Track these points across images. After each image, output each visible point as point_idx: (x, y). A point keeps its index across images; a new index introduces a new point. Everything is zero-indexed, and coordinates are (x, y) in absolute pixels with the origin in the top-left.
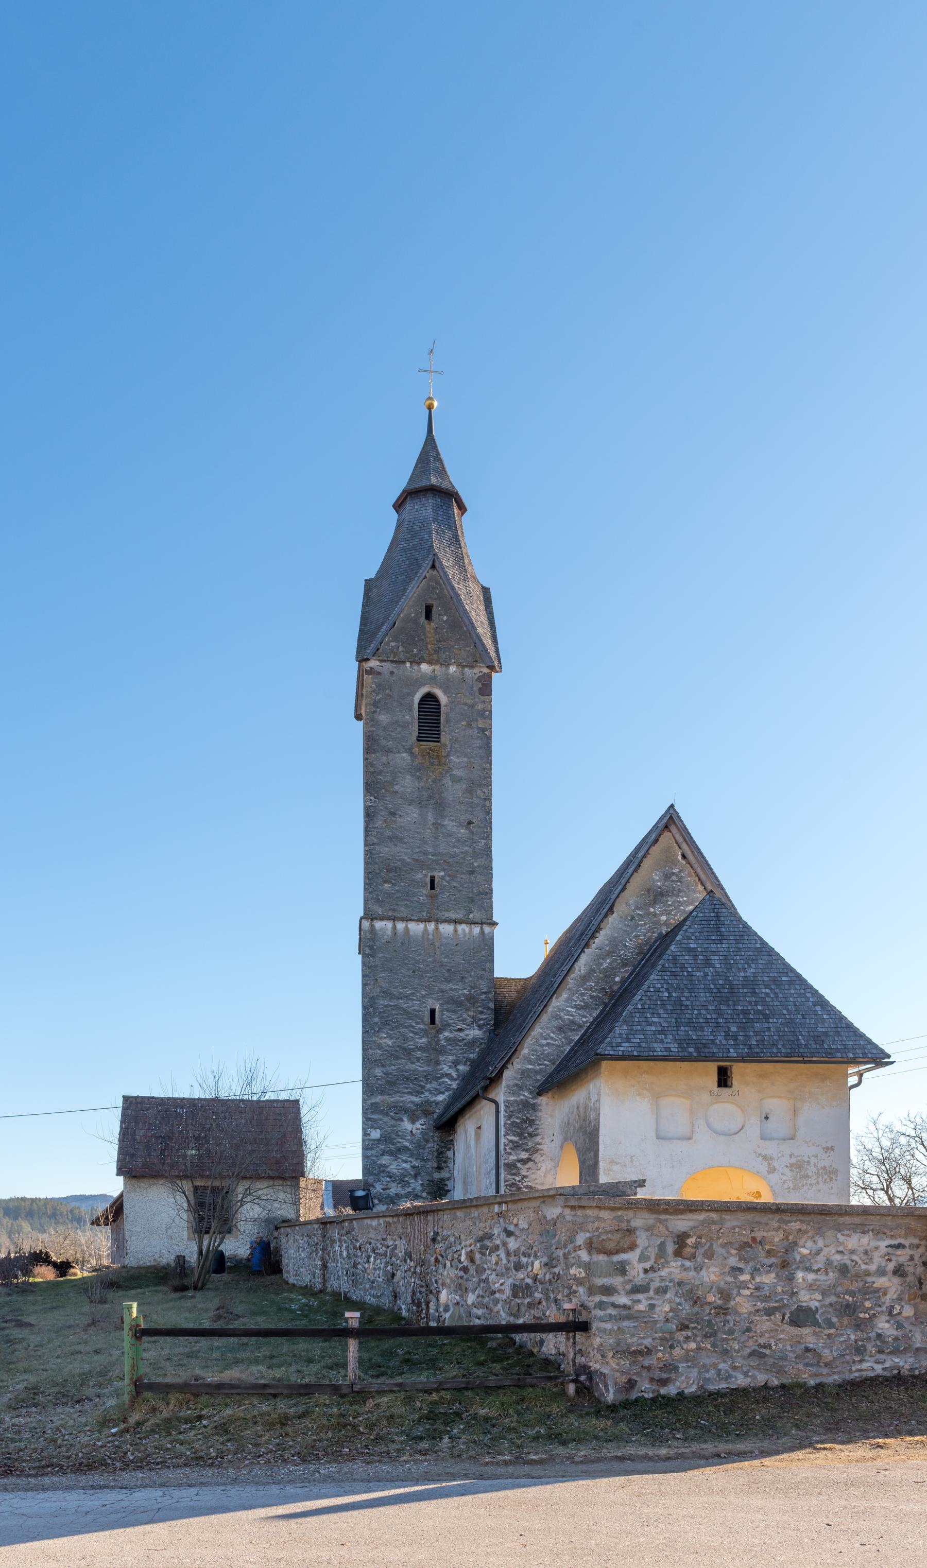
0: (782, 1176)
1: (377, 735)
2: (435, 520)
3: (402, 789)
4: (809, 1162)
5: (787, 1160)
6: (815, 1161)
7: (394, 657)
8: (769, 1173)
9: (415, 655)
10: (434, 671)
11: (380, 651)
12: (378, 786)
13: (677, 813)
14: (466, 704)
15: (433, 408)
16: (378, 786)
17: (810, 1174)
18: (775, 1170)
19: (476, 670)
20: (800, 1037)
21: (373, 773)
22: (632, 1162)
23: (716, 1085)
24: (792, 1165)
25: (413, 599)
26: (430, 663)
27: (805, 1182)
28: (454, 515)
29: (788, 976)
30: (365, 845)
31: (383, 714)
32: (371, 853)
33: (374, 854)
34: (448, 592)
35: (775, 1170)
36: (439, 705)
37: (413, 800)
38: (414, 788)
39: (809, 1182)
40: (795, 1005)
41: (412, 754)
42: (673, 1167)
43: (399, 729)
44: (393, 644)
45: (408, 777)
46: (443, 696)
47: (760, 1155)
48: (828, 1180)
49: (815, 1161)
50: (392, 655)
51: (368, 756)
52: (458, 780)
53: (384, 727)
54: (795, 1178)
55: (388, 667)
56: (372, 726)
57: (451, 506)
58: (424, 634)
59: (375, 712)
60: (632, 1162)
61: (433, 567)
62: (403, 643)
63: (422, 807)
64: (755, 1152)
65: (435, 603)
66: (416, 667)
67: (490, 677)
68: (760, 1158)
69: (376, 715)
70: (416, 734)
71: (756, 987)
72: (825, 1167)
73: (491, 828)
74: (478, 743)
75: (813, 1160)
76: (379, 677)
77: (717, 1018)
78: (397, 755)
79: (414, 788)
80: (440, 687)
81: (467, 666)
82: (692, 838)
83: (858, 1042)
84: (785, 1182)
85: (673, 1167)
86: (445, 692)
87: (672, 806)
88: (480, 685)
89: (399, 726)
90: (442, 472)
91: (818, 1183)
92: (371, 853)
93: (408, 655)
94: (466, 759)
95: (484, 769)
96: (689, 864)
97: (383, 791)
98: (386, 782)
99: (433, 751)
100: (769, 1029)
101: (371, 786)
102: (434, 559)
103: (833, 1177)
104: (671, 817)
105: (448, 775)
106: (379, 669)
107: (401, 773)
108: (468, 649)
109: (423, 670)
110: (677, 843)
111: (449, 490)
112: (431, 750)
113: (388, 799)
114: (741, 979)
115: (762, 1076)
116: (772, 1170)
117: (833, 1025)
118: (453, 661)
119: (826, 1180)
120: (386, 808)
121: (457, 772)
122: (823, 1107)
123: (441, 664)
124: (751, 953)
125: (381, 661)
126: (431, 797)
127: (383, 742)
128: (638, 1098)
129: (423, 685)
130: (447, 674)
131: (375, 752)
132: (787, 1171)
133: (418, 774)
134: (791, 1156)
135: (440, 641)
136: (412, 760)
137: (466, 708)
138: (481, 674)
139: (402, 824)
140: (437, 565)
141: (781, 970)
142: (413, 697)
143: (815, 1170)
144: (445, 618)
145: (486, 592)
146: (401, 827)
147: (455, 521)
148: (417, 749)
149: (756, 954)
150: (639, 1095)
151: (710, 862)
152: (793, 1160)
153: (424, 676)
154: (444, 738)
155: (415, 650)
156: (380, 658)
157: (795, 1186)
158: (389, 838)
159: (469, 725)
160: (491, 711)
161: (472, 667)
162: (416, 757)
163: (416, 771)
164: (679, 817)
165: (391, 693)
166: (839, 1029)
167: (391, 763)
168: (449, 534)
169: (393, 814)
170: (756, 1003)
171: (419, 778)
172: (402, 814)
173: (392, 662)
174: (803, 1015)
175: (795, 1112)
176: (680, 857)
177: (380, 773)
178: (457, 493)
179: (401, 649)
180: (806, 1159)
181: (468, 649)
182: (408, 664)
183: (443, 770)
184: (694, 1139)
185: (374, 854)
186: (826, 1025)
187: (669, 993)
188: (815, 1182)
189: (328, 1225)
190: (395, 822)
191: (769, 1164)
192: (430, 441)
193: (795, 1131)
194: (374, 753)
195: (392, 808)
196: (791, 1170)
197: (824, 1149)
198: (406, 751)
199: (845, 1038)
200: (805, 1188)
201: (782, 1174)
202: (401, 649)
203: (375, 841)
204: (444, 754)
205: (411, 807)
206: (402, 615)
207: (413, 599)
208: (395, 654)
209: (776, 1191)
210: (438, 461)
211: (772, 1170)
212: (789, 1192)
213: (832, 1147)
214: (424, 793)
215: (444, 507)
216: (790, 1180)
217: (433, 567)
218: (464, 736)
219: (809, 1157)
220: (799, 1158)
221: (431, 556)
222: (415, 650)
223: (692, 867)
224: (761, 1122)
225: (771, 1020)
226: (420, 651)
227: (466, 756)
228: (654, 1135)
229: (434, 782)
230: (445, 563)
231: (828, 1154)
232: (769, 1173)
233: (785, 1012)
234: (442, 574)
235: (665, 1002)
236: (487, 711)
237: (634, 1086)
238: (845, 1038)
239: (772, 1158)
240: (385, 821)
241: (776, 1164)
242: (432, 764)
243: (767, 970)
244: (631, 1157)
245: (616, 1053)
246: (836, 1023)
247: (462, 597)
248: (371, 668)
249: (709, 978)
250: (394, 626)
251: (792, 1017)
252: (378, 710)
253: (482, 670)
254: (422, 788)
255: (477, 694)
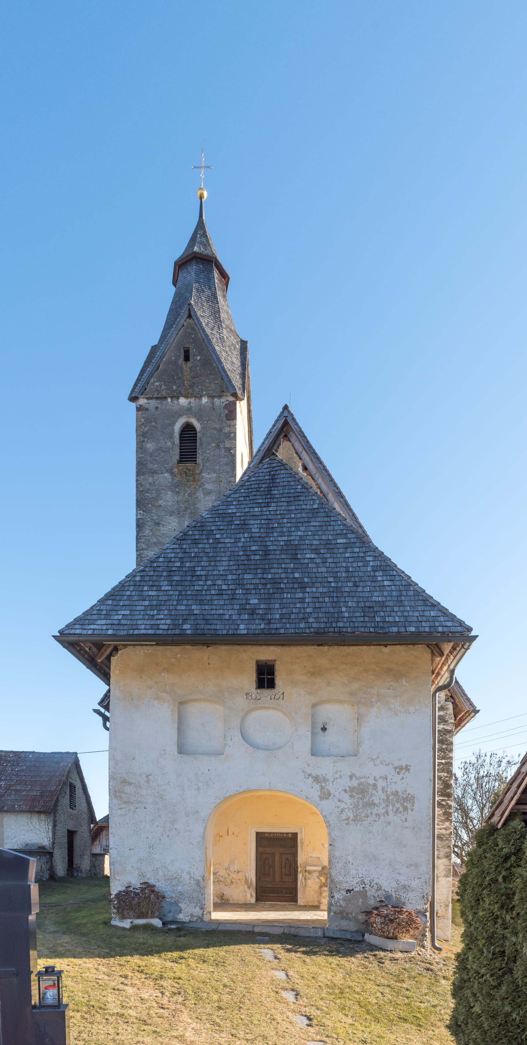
0: (339, 804)
1: (145, 460)
2: (197, 282)
3: (165, 503)
4: (375, 786)
5: (345, 783)
6: (384, 784)
7: (158, 394)
8: (322, 798)
9: (174, 391)
10: (190, 403)
11: (147, 390)
12: (146, 502)
13: (292, 415)
14: (215, 429)
15: (203, 197)
16: (146, 502)
17: (377, 801)
18: (329, 795)
19: (223, 400)
20: (344, 609)
21: (142, 491)
22: (148, 782)
23: (254, 685)
24: (352, 789)
25: (174, 344)
26: (186, 397)
27: (369, 811)
28: (214, 278)
29: (347, 538)
30: (137, 551)
31: (150, 443)
32: (141, 557)
33: (143, 557)
34: (202, 336)
35: (329, 795)
36: (196, 430)
37: (173, 512)
38: (174, 502)
39: (375, 812)
40: (348, 571)
41: (172, 474)
42: (198, 789)
43: (162, 454)
44: (157, 384)
45: (169, 493)
46: (197, 424)
47: (310, 775)
48: (401, 809)
49: (384, 784)
50: (156, 393)
51: (138, 478)
52: (209, 493)
53: (151, 453)
54: (356, 806)
55: (153, 403)
56: (141, 453)
57: (211, 271)
58: (182, 373)
59: (143, 441)
60: (148, 782)
61: (190, 316)
62: (165, 382)
63: (180, 517)
64: (303, 772)
65: (191, 346)
66: (175, 402)
67: (235, 404)
68: (311, 780)
69: (144, 444)
70: (177, 457)
71: (298, 552)
72: (397, 792)
73: (137, 468)
74: (224, 460)
75: (381, 784)
76: (147, 412)
77: (235, 589)
78: (160, 476)
79: (174, 502)
80: (195, 417)
81: (216, 396)
82: (308, 442)
83: (427, 614)
84: (342, 811)
85: (198, 789)
86: (198, 420)
87: (286, 408)
88: (227, 412)
89: (162, 451)
90: (207, 244)
91: (387, 813)
92: (141, 557)
93: (169, 391)
94: (215, 475)
95: (230, 482)
96: (311, 475)
97: (150, 505)
98: (152, 498)
99: (189, 470)
100: (302, 600)
101: (141, 503)
102: (189, 309)
103: (409, 806)
104: (286, 420)
105: (201, 489)
106: (147, 406)
107: (163, 489)
108: (217, 382)
109: (181, 403)
110: (297, 453)
111: (209, 256)
112: (187, 469)
113: (154, 512)
114: (282, 543)
115: (315, 673)
116: (326, 795)
117: (394, 593)
118: (204, 393)
119: (398, 809)
120: (152, 519)
121: (208, 486)
122: (396, 714)
123: (195, 397)
124: (304, 515)
125: (148, 399)
126: (187, 508)
127: (150, 466)
128: (156, 702)
129: (180, 416)
130: (200, 405)
131: (143, 474)
132: (346, 797)
133: (177, 490)
134: (351, 777)
135: (195, 378)
136: (172, 479)
137: (215, 432)
138: (227, 402)
139: (165, 532)
140: (192, 313)
141: (339, 532)
142: (174, 426)
143: (383, 796)
144: (199, 358)
145: (244, 346)
146: (164, 534)
147: (214, 283)
148: (176, 470)
149: (311, 515)
150: (157, 698)
151: (328, 468)
152: (355, 783)
153: (182, 408)
154: (199, 460)
155: (174, 387)
156: (147, 396)
157: (356, 817)
158: (155, 543)
159: (218, 446)
160: (235, 433)
161: (220, 397)
162: (175, 476)
163: (175, 488)
164: (294, 419)
165: (156, 425)
166: (403, 598)
167: (156, 483)
168: (208, 292)
169: (158, 524)
170: (294, 570)
171: (178, 493)
172: (164, 524)
173: (157, 398)
174: (355, 582)
175: (359, 719)
176: (300, 469)
177: (148, 491)
178: (216, 258)
179: (163, 387)
180: (371, 781)
181: (217, 382)
182: (169, 400)
183: (197, 485)
184: (225, 754)
185: (143, 557)
186: (386, 593)
187: (182, 563)
188: (383, 811)
189: (337, 854)
190: (159, 530)
191: (322, 788)
192: (201, 225)
193: (359, 744)
194: (143, 475)
195: (157, 519)
196: (351, 796)
197: (395, 768)
198: (167, 471)
199: (408, 608)
200: (370, 819)
201: (339, 801)
202: (163, 387)
203: (144, 546)
204: (197, 472)
205: (172, 518)
206: (164, 359)
207: (174, 344)
208: (159, 392)
209: (331, 823)
210: (204, 237)
211: (326, 795)
212: (347, 824)
213: (407, 766)
214: (182, 505)
215: (206, 272)
216: (349, 809)
217: (190, 316)
218: (214, 456)
219: (375, 779)
220: (362, 780)
221: (186, 306)
222: (174, 387)
223: (313, 479)
224: (313, 734)
225: (308, 590)
226: (178, 387)
227: (215, 472)
228: (175, 749)
229: (190, 495)
230: (199, 313)
231: (401, 775)
232: (322, 798)
233: (331, 579)
234: (196, 321)
235: (172, 573)
236: (232, 433)
237: (151, 688)
238: (408, 608)
239: (325, 780)
240: (151, 530)
241: (331, 787)
242: (188, 481)
243: (320, 533)
244: (147, 777)
245: (84, 632)
246: (400, 591)
247: (214, 341)
248: (141, 406)
249: (240, 544)
250: (158, 369)
251: (340, 585)
252: (146, 440)
253: (228, 399)
254: (181, 501)
255: (224, 419)
